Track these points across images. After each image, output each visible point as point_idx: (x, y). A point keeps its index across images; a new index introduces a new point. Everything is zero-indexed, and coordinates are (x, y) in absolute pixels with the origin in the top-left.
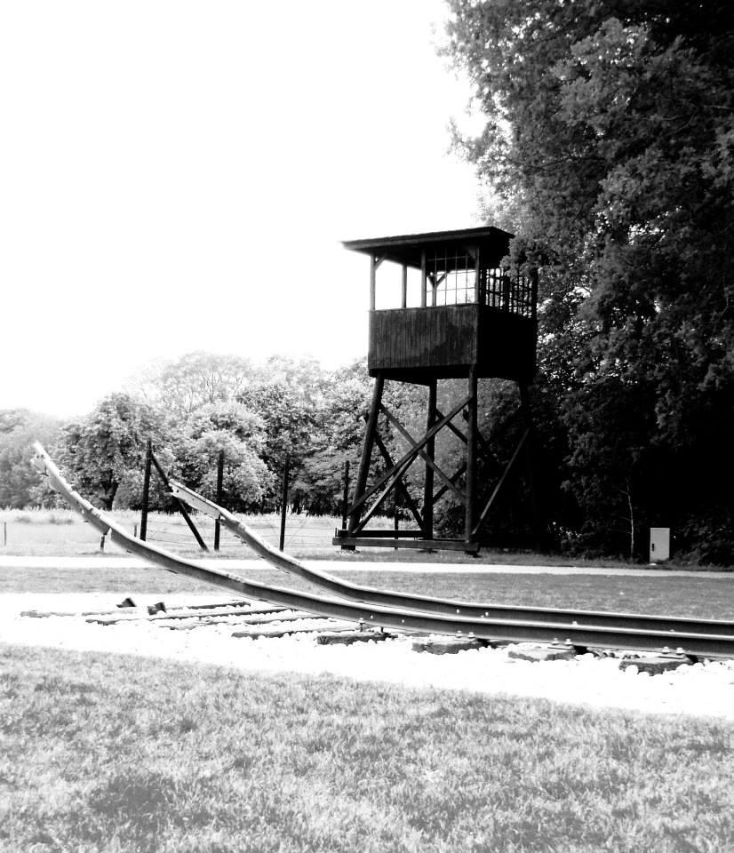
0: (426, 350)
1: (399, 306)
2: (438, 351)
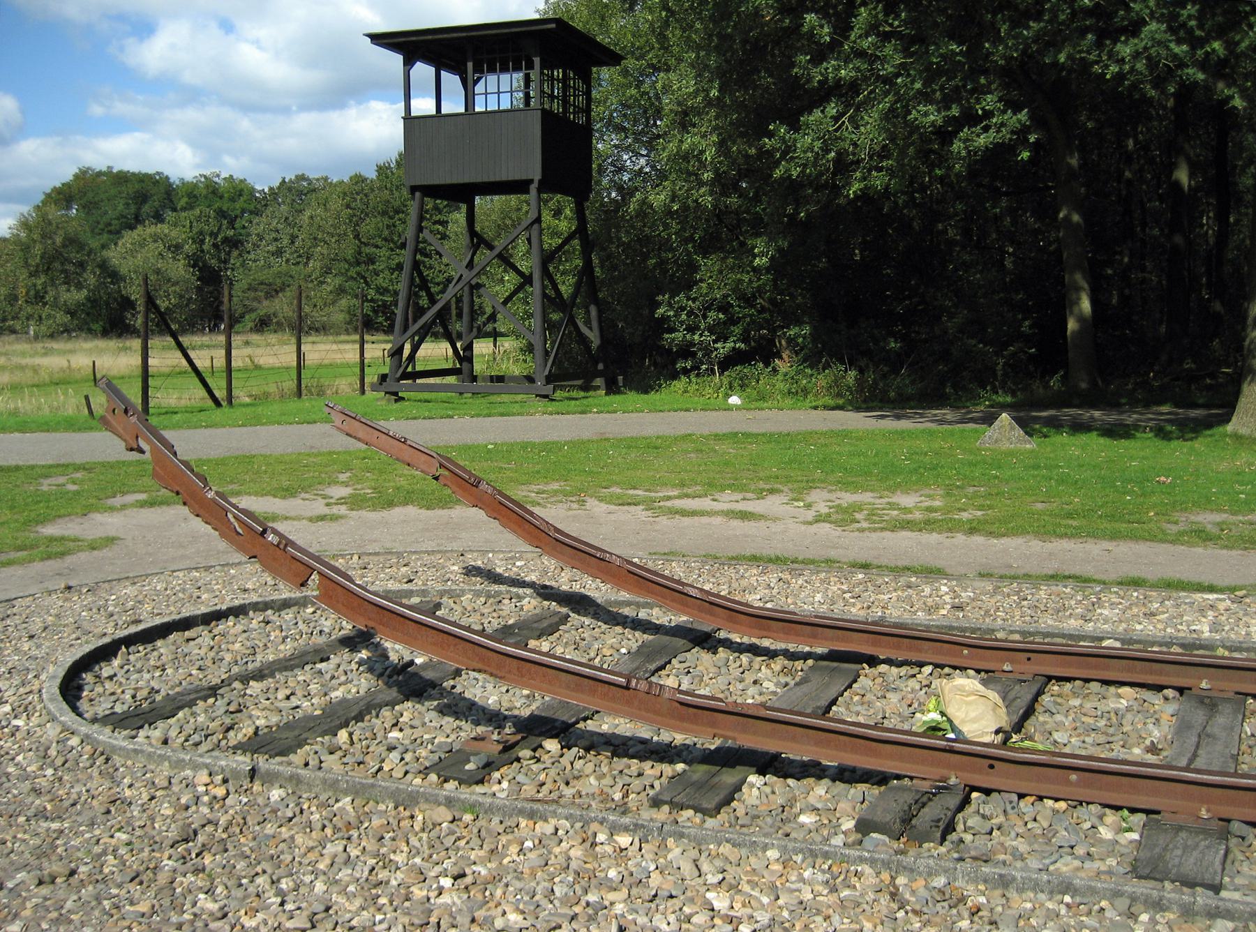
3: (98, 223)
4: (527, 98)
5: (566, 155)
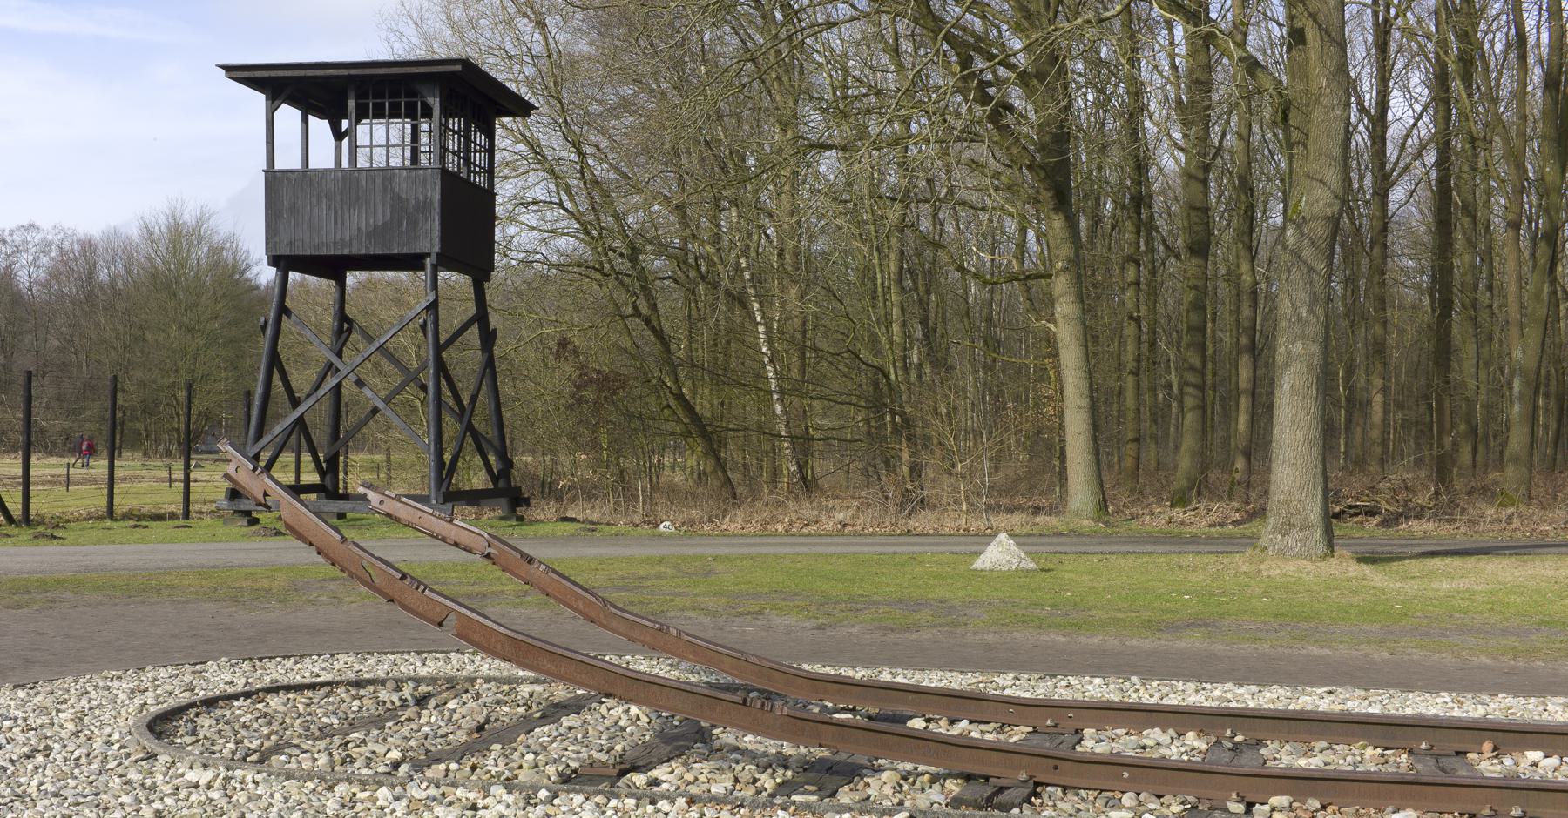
0: (359, 229)
1: (298, 165)
2: (379, 232)
3: (28, 592)
4: (415, 153)
5: (467, 223)
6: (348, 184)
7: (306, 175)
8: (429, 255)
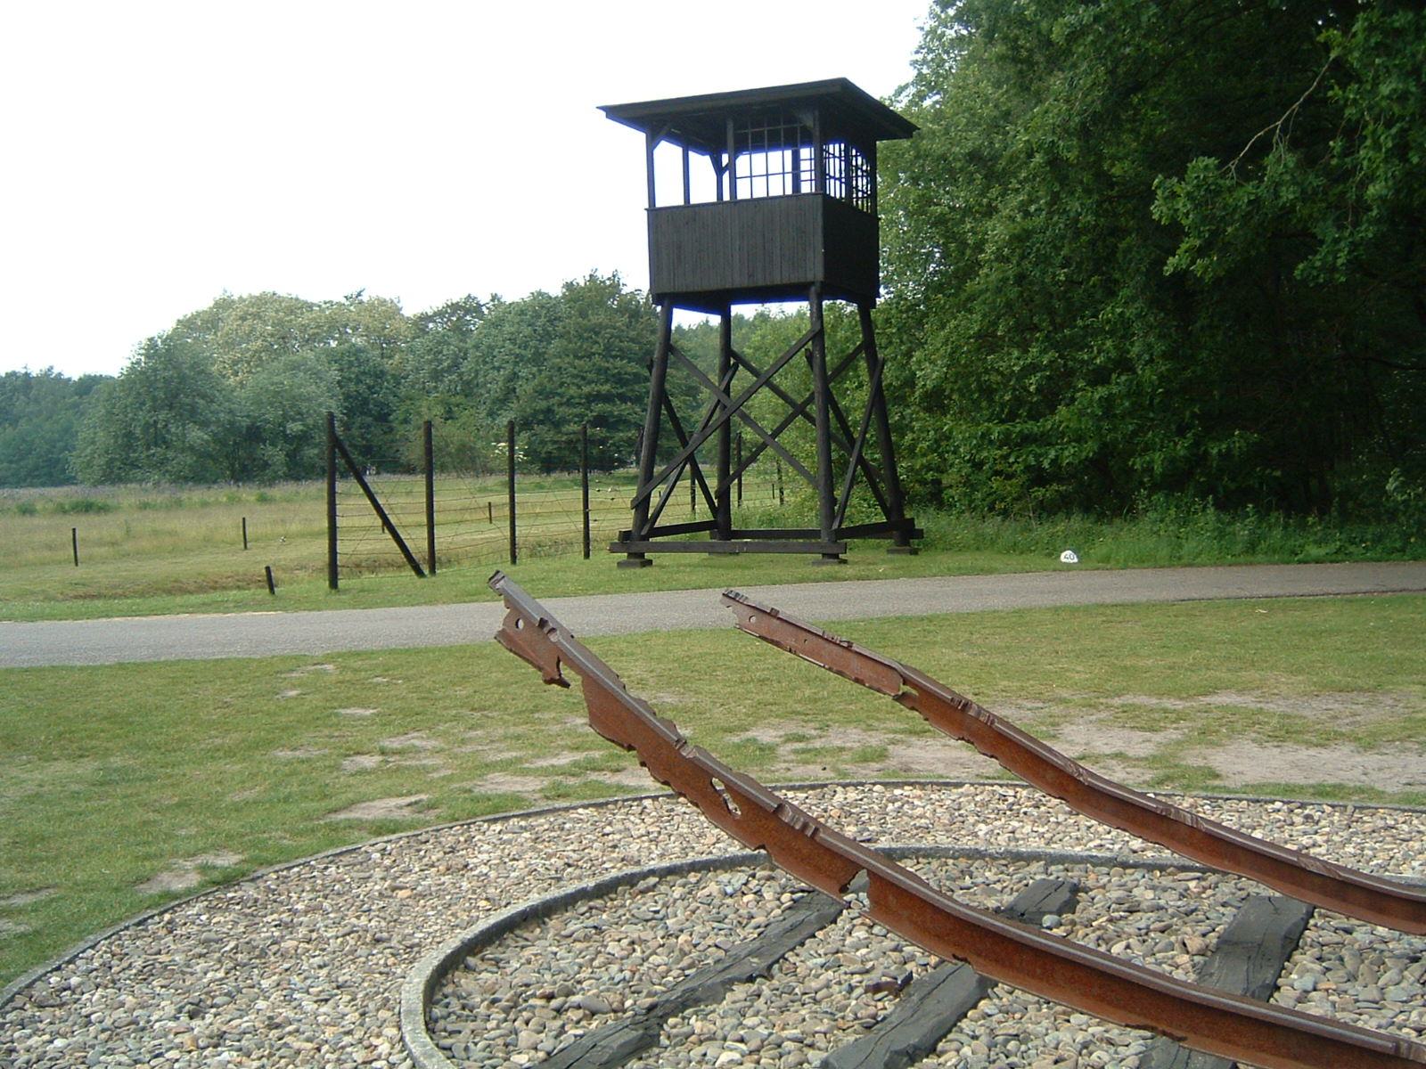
6: (731, 212)
7: (689, 212)
8: (812, 283)
